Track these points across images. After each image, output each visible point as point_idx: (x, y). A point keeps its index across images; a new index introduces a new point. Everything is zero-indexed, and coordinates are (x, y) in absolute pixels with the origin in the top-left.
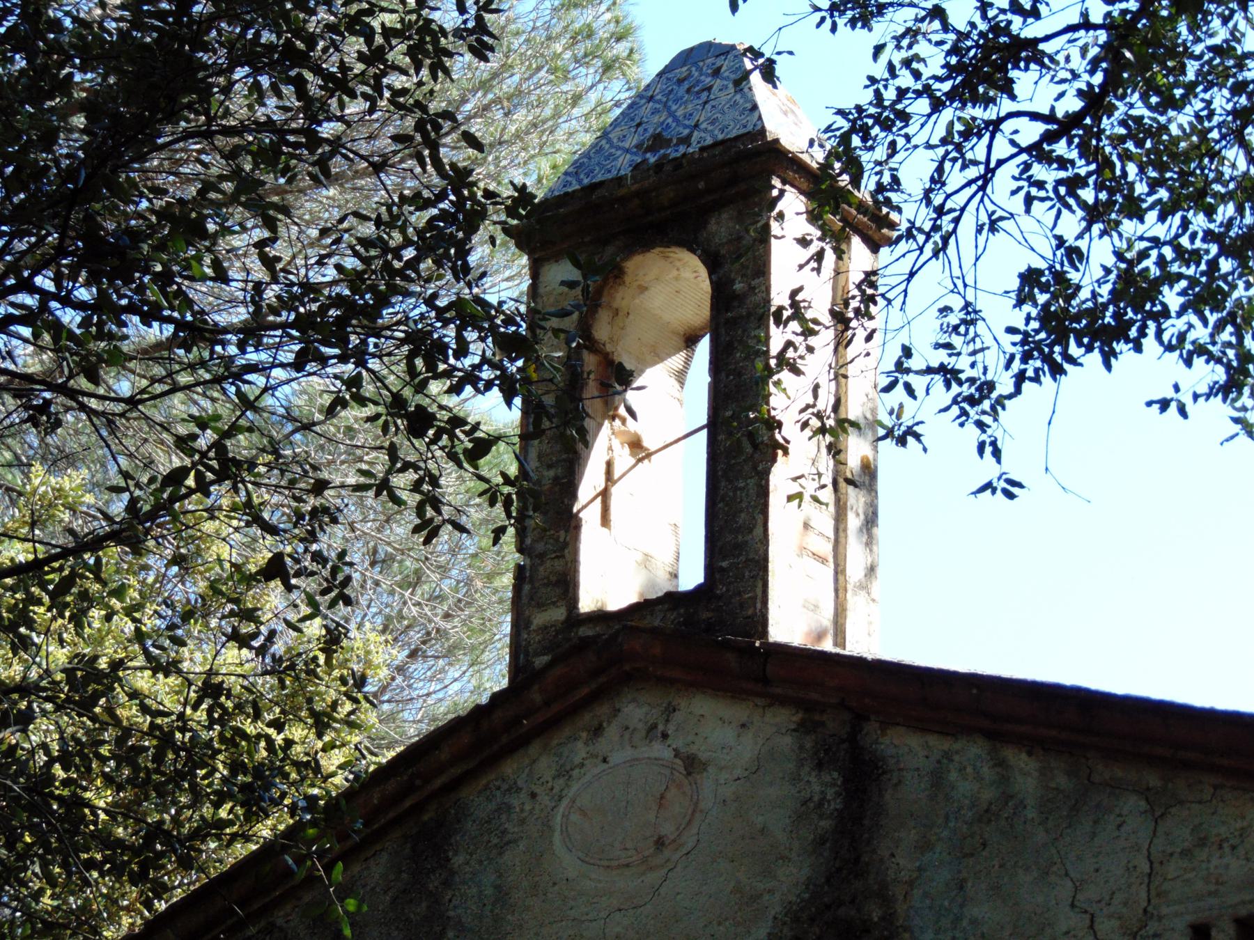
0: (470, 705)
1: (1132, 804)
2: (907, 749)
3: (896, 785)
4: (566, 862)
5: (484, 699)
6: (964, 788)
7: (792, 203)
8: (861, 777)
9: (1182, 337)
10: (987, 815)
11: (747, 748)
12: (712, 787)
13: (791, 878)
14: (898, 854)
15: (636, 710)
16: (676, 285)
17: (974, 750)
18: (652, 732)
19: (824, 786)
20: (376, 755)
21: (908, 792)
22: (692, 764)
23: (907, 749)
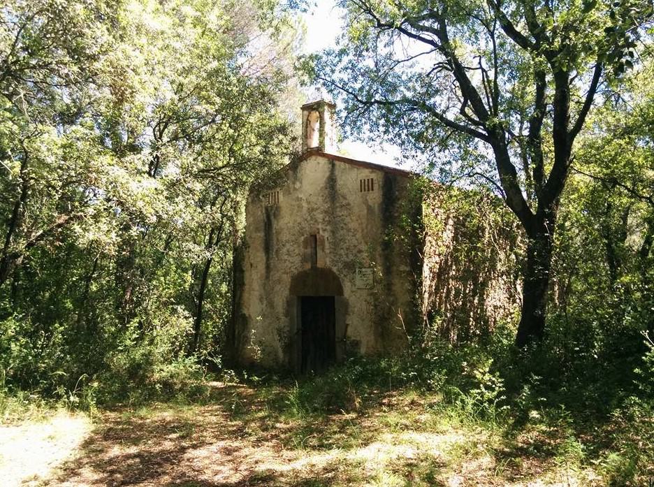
0: (246, 282)
1: (356, 169)
2: (337, 163)
3: (262, 298)
4: (307, 172)
5: (264, 238)
6: (342, 166)
7: (326, 108)
8: (333, 165)
9: (285, 262)
10: (344, 169)
11: (323, 162)
12: (320, 165)
13: (328, 174)
14: (336, 173)
15: (314, 158)
16: (315, 114)
17: (342, 163)
18: (315, 160)
19: (330, 166)
20: (212, 357)
21: (337, 167)
22: (319, 163)
23: (337, 163)
